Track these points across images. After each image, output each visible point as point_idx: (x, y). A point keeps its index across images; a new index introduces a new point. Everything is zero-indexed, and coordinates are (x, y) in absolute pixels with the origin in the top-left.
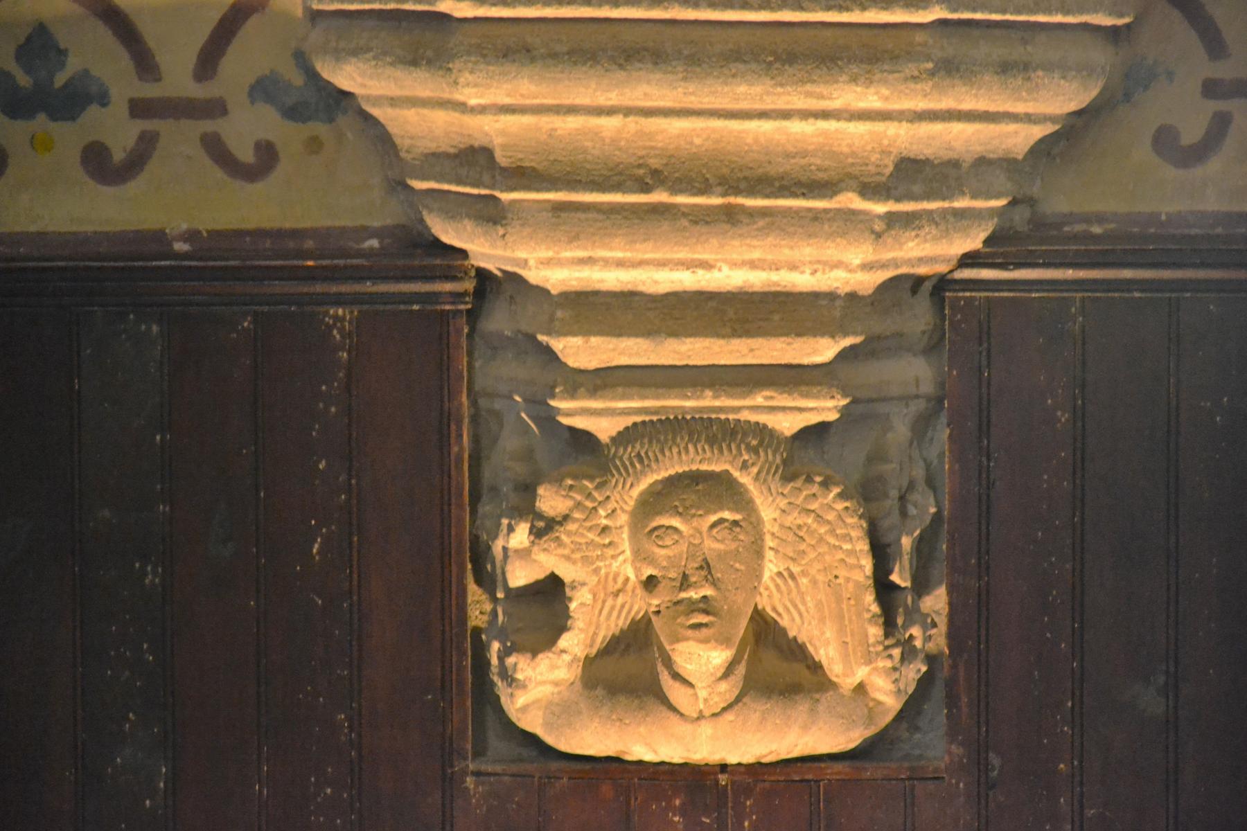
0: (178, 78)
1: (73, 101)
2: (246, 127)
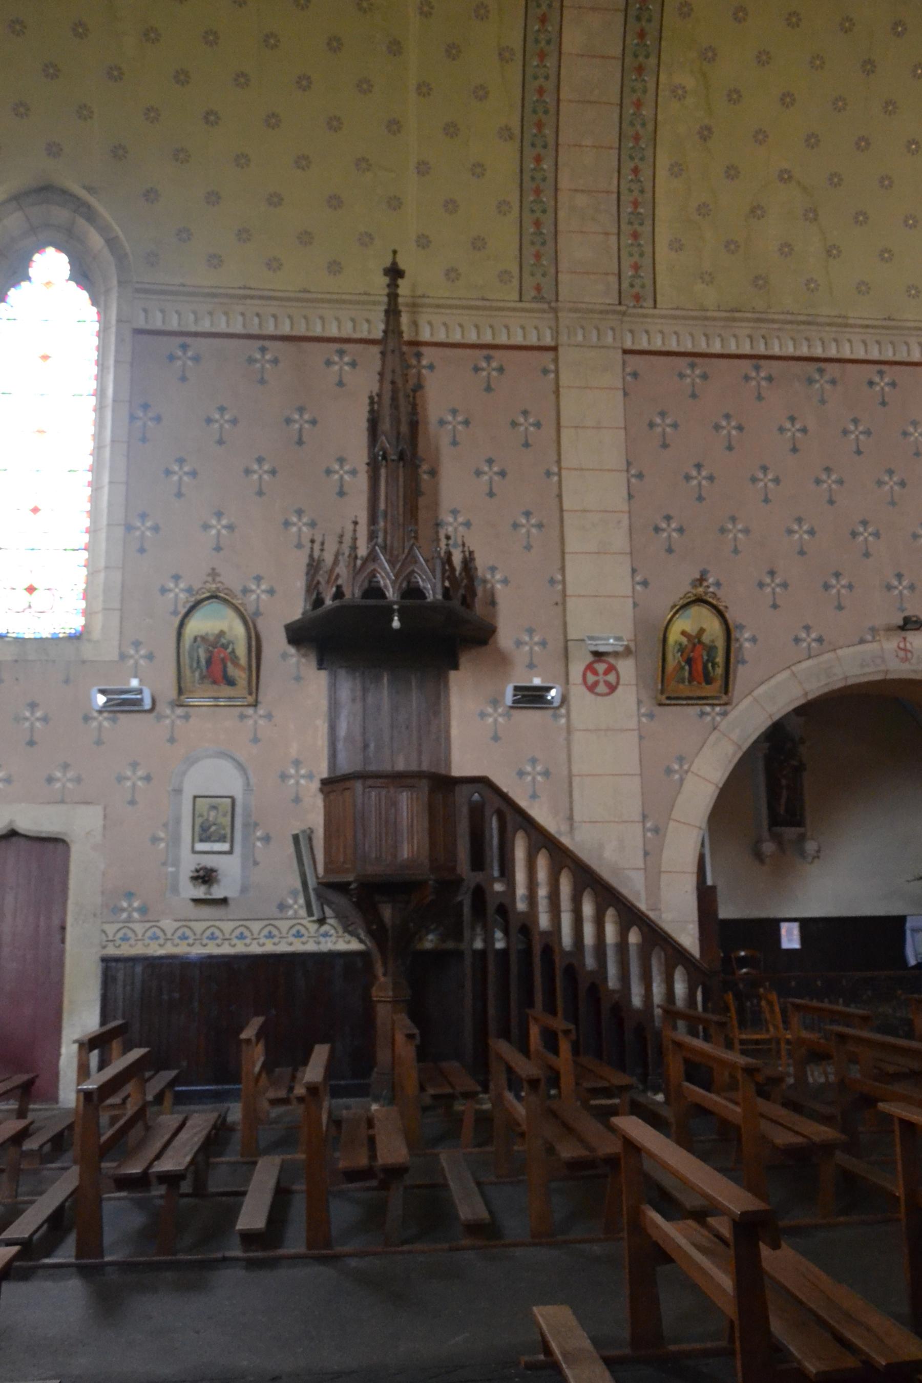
0: (169, 936)
1: (303, 936)
2: (118, 942)
